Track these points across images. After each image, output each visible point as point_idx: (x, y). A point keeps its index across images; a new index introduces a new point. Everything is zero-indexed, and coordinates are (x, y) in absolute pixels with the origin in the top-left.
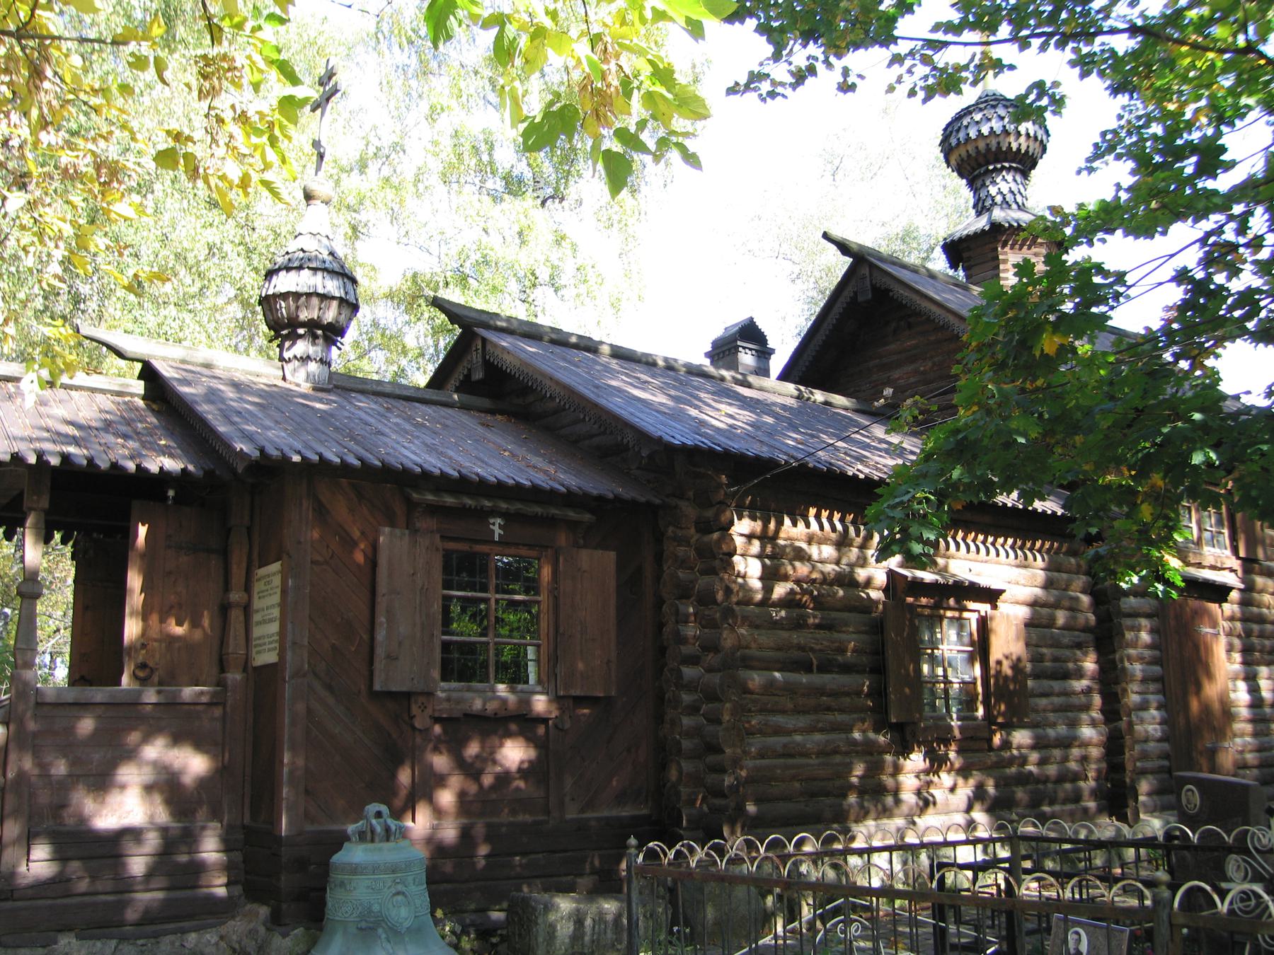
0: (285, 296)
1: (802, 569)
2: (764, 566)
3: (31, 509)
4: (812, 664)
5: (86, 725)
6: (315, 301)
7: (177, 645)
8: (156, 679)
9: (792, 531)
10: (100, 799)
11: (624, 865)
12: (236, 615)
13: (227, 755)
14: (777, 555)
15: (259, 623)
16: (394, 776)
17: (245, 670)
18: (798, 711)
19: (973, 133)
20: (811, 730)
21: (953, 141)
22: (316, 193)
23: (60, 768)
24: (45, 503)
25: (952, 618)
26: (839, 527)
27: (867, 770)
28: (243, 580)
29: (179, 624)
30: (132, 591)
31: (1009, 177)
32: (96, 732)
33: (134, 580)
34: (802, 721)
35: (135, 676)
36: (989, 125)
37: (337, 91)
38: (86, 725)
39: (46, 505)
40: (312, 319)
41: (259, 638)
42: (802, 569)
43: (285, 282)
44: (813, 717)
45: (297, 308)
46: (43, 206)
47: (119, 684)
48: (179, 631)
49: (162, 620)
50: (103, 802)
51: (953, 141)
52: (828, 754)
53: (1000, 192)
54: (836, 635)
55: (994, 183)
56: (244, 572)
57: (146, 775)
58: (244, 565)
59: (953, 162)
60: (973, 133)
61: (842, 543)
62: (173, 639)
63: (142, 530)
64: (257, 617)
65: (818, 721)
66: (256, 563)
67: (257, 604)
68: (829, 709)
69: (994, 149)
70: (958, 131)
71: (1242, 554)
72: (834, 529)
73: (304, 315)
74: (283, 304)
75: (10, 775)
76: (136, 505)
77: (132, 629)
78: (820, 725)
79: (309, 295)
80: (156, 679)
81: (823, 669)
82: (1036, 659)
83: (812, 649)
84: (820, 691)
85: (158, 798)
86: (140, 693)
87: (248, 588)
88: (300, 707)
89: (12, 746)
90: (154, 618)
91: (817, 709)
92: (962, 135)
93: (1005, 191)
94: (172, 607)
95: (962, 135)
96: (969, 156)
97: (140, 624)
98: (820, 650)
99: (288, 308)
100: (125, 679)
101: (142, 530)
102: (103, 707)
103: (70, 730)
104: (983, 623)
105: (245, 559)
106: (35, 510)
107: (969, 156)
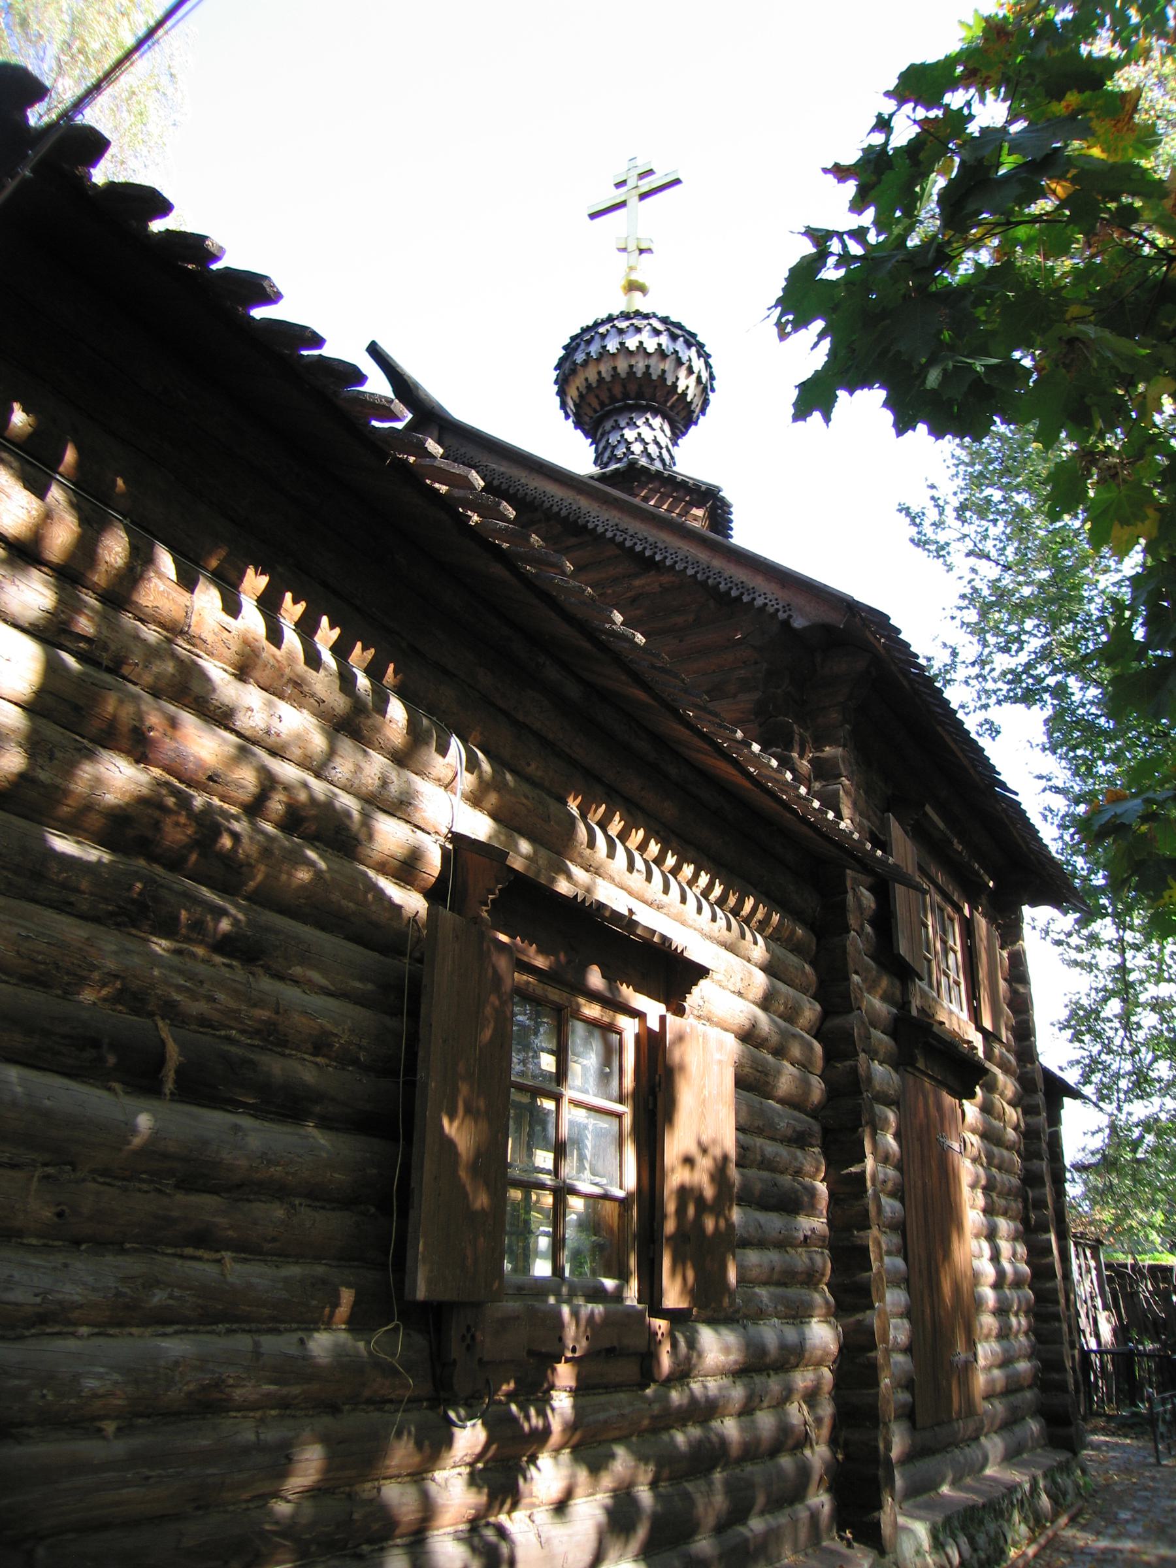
1: (204, 745)
2: (52, 668)
4: (161, 1060)
9: (212, 618)
11: (1098, 260)
14: (108, 659)
18: (70, 1236)
19: (612, 346)
20: (124, 1314)
21: (580, 357)
25: (593, 1023)
26: (363, 682)
27: (332, 1465)
31: (657, 422)
34: (81, 1279)
36: (638, 338)
42: (204, 745)
44: (133, 1265)
46: (1129, 1239)
51: (580, 357)
52: (170, 1415)
53: (640, 438)
54: (266, 984)
55: (632, 424)
59: (573, 392)
60: (612, 346)
61: (351, 725)
65: (152, 1283)
68: (203, 1239)
69: (639, 375)
70: (589, 342)
72: (346, 680)
78: (159, 1297)
81: (197, 1088)
82: (741, 1147)
83: (170, 1010)
84: (193, 1172)
91: (153, 1238)
92: (594, 349)
93: (649, 439)
95: (594, 349)
96: (601, 380)
98: (204, 1022)
104: (653, 1048)
107: (601, 380)
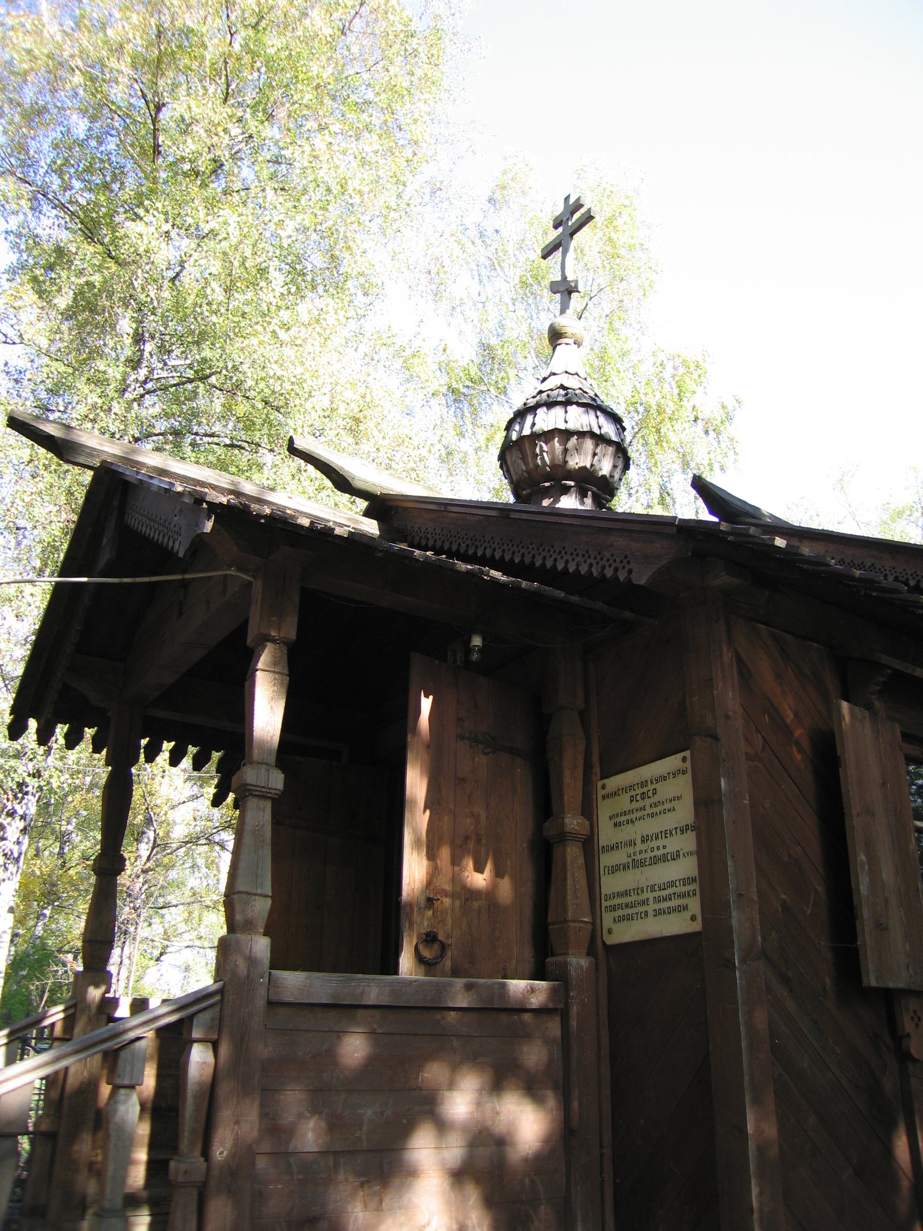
0: (548, 436)
3: (265, 639)
5: (355, 1048)
6: (589, 444)
7: (476, 905)
8: (448, 963)
10: (373, 1204)
12: (573, 854)
13: (575, 1105)
15: (614, 869)
16: (888, 1152)
17: (591, 952)
22: (569, 330)
23: (310, 1136)
24: (290, 631)
28: (580, 797)
29: (479, 869)
30: (414, 802)
32: (371, 1062)
33: (416, 784)
35: (419, 958)
37: (592, 218)
38: (355, 1048)
39: (293, 635)
40: (584, 468)
41: (615, 895)
43: (546, 420)
45: (566, 451)
47: (395, 970)
48: (480, 880)
49: (456, 861)
50: (379, 1209)
56: (580, 784)
57: (454, 1150)
58: (580, 772)
62: (469, 895)
63: (426, 704)
64: (606, 860)
66: (597, 770)
67: (606, 834)
71: (46, 1046)
73: (577, 461)
74: (545, 448)
75: (221, 1152)
76: (417, 662)
77: (414, 870)
79: (581, 434)
80: (448, 963)
85: (473, 1195)
86: (441, 990)
87: (588, 810)
88: (761, 1018)
89: (224, 1089)
90: (445, 853)
94: (467, 838)
97: (425, 862)
99: (552, 452)
100: (406, 962)
101: (426, 704)
102: (377, 1013)
103: (329, 1056)
105: (581, 761)
106: (273, 641)
